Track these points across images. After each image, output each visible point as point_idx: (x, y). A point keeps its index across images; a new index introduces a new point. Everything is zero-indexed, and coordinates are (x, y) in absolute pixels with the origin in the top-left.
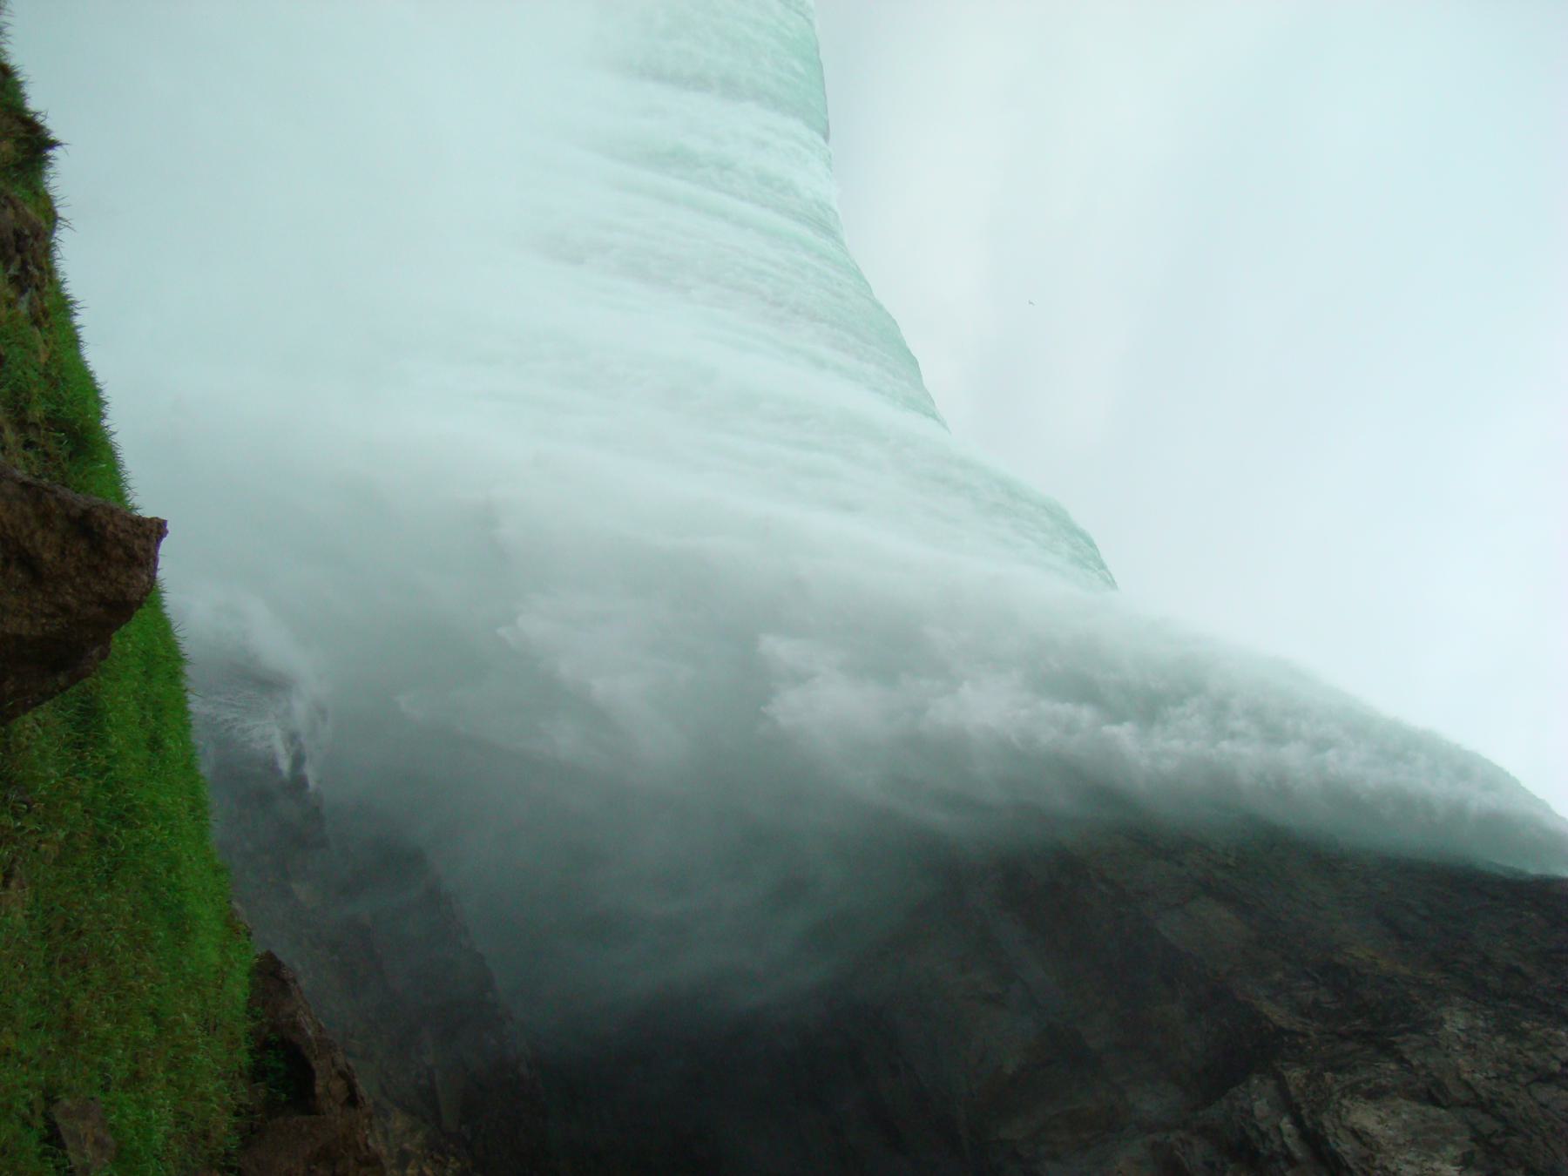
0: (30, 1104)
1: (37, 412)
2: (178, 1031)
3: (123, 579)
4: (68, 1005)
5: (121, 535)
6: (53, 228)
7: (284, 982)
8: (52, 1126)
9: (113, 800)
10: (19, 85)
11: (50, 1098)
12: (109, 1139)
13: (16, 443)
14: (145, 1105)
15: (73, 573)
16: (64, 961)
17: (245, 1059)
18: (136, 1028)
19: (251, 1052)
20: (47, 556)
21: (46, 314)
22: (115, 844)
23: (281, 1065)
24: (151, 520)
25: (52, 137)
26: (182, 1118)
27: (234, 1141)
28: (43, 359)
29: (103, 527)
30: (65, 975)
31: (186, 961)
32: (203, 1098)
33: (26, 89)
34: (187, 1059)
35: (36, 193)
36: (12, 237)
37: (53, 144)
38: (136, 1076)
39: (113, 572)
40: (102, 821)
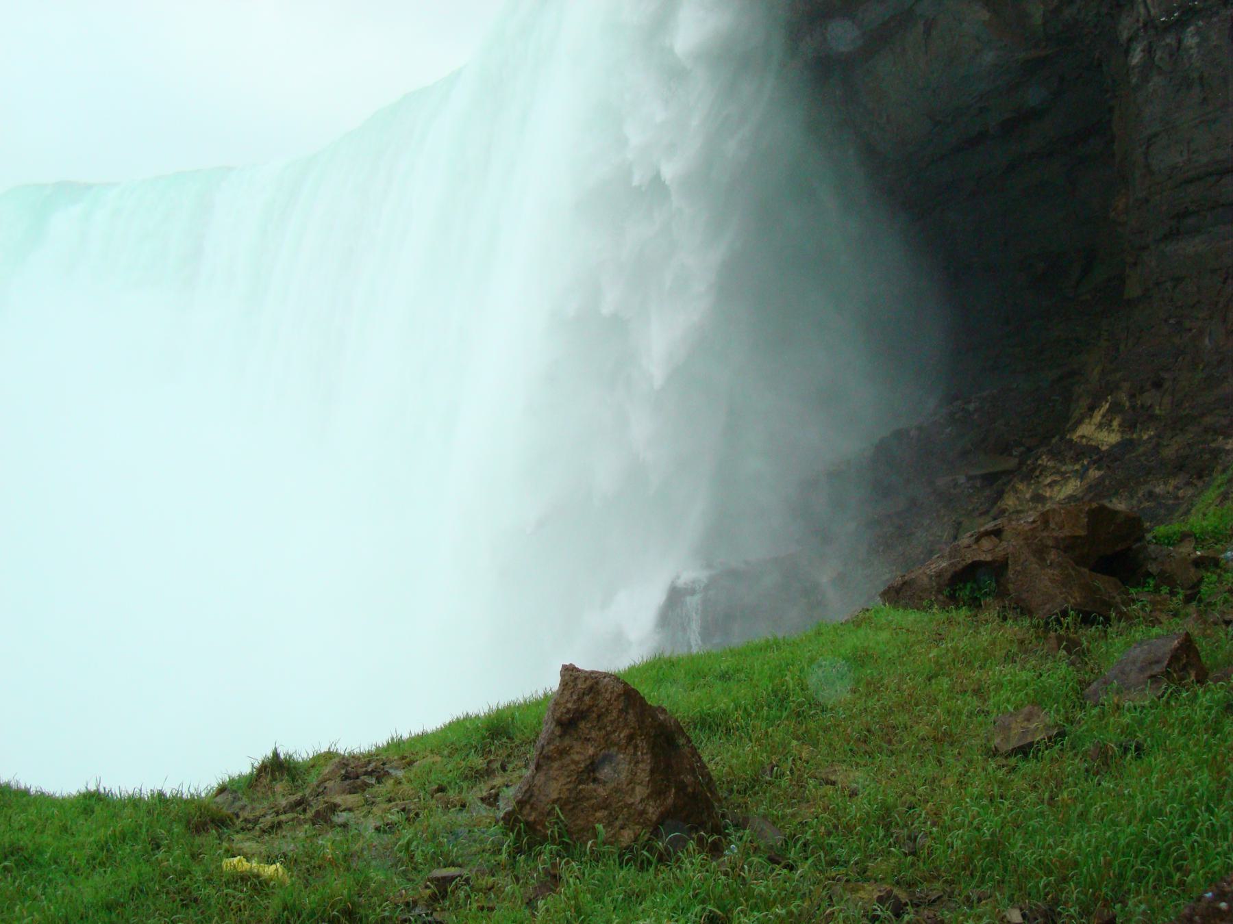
0: (999, 767)
1: (479, 762)
2: (942, 661)
3: (608, 696)
4: (923, 739)
5: (575, 697)
6: (336, 754)
7: (905, 583)
8: (1014, 752)
9: (769, 706)
10: (232, 780)
11: (995, 753)
12: (1026, 710)
13: (502, 776)
14: (1000, 685)
15: (603, 732)
16: (890, 742)
17: (964, 613)
18: (941, 691)
19: (957, 608)
20: (591, 751)
22: (801, 705)
23: (969, 586)
24: (563, 676)
25: (270, 754)
26: (1010, 658)
27: (1026, 622)
28: (438, 759)
29: (568, 711)
30: (901, 742)
31: (890, 655)
32: (993, 643)
33: (235, 774)
34: (964, 654)
35: (313, 766)
36: (348, 782)
37: (276, 755)
38: (976, 692)
39: (602, 703)
40: (785, 714)
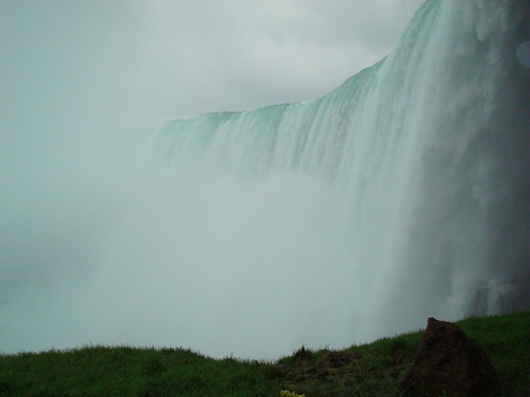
1: (390, 358)
10: (285, 358)
21: (357, 354)
25: (301, 349)
28: (372, 355)
35: (318, 355)
36: (332, 363)
37: (303, 349)
